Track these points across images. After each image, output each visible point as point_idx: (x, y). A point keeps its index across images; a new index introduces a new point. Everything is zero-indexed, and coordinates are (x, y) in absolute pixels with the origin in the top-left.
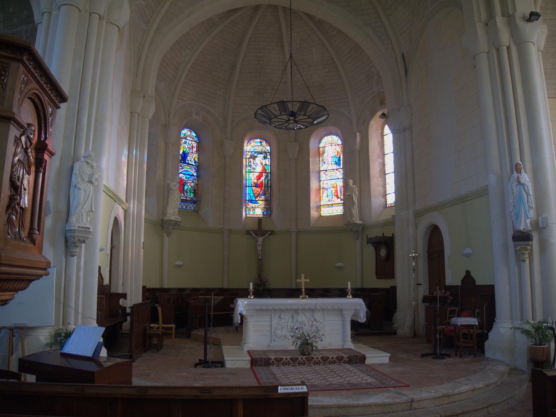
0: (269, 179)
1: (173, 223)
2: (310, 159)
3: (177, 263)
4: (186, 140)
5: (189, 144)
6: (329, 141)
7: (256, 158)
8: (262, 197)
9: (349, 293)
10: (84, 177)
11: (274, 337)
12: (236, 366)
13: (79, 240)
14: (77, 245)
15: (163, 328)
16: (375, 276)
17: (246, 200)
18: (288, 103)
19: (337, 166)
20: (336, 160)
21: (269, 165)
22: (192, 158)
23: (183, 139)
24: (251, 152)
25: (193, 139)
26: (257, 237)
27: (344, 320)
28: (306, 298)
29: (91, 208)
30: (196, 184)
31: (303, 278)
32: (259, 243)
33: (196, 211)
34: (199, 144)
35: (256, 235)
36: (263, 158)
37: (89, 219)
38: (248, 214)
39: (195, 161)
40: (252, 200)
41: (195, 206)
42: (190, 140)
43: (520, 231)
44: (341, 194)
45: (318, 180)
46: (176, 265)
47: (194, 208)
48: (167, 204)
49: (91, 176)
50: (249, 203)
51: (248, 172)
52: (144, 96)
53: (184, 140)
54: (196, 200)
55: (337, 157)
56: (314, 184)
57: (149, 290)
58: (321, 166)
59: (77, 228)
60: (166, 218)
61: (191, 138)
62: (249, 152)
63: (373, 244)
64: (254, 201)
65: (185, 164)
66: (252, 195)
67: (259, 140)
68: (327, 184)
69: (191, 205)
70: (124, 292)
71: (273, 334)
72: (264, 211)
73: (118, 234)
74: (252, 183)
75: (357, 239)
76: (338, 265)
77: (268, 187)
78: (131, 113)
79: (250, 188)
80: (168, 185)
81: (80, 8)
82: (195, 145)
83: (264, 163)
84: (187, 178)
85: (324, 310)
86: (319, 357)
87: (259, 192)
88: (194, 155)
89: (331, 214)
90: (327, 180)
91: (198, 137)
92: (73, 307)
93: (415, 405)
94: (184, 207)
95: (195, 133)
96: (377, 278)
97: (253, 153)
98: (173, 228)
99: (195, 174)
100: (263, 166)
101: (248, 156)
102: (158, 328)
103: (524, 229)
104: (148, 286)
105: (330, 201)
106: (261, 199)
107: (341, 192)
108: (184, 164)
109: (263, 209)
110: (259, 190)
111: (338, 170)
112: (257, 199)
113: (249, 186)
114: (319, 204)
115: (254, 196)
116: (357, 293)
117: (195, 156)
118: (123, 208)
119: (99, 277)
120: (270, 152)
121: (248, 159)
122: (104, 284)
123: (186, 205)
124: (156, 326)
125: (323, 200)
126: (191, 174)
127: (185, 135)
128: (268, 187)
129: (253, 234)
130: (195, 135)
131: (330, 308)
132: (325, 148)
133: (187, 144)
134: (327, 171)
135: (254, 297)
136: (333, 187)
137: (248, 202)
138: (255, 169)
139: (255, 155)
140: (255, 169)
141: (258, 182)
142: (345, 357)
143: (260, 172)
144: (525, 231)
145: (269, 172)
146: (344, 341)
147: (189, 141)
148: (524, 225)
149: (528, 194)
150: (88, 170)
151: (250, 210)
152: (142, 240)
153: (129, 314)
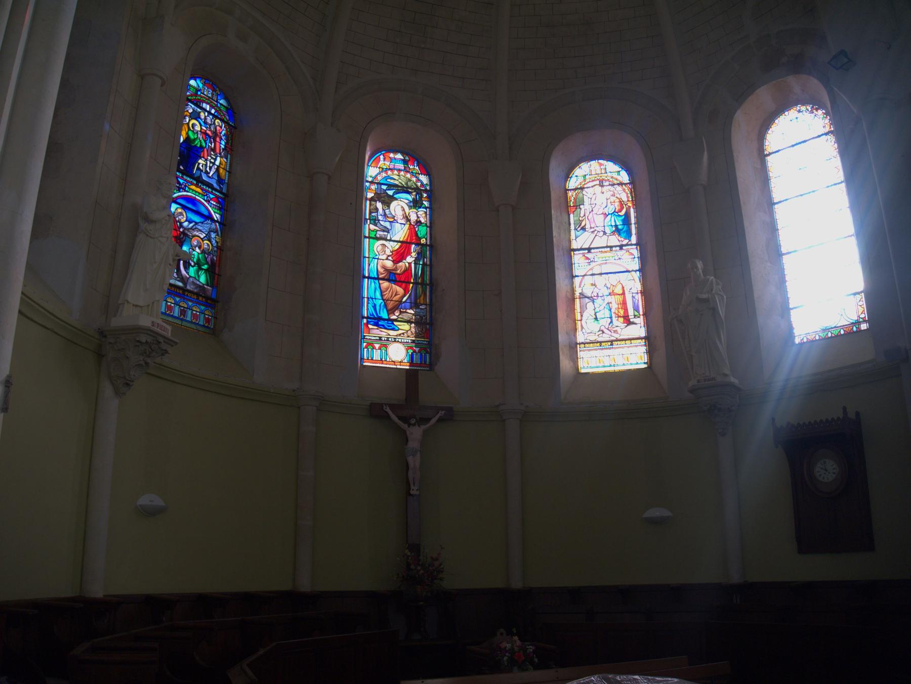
0: (428, 263)
2: (553, 212)
3: (145, 500)
6: (593, 173)
7: (393, 201)
8: (408, 311)
19: (620, 239)
20: (618, 223)
21: (428, 224)
24: (378, 184)
25: (220, 114)
26: (406, 426)
30: (217, 247)
32: (413, 444)
33: (213, 330)
35: (405, 420)
36: (412, 204)
38: (365, 358)
39: (219, 176)
40: (380, 319)
42: (209, 113)
44: (636, 313)
46: (140, 505)
47: (208, 320)
50: (370, 326)
51: (369, 237)
54: (214, 297)
55: (619, 214)
58: (573, 236)
60: (116, 322)
61: (212, 107)
62: (372, 183)
64: (385, 320)
65: (188, 179)
66: (379, 302)
67: (399, 156)
68: (592, 285)
72: (414, 351)
79: (373, 285)
83: (413, 218)
84: (190, 222)
87: (398, 297)
88: (218, 159)
89: (611, 369)
90: (593, 275)
94: (176, 312)
95: (226, 99)
97: (384, 187)
98: (142, 363)
99: (216, 216)
100: (410, 224)
105: (606, 331)
106: (405, 317)
107: (636, 309)
108: (187, 176)
109: (411, 348)
110: (400, 290)
111: (624, 248)
112: (394, 317)
113: (371, 278)
115: (386, 306)
117: (220, 163)
123: (181, 304)
125: (582, 327)
126: (206, 213)
127: (196, 95)
128: (423, 284)
129: (394, 417)
134: (592, 251)
137: (368, 323)
138: (388, 232)
139: (390, 193)
140: (388, 232)
143: (401, 240)
147: (206, 114)
151: (374, 348)
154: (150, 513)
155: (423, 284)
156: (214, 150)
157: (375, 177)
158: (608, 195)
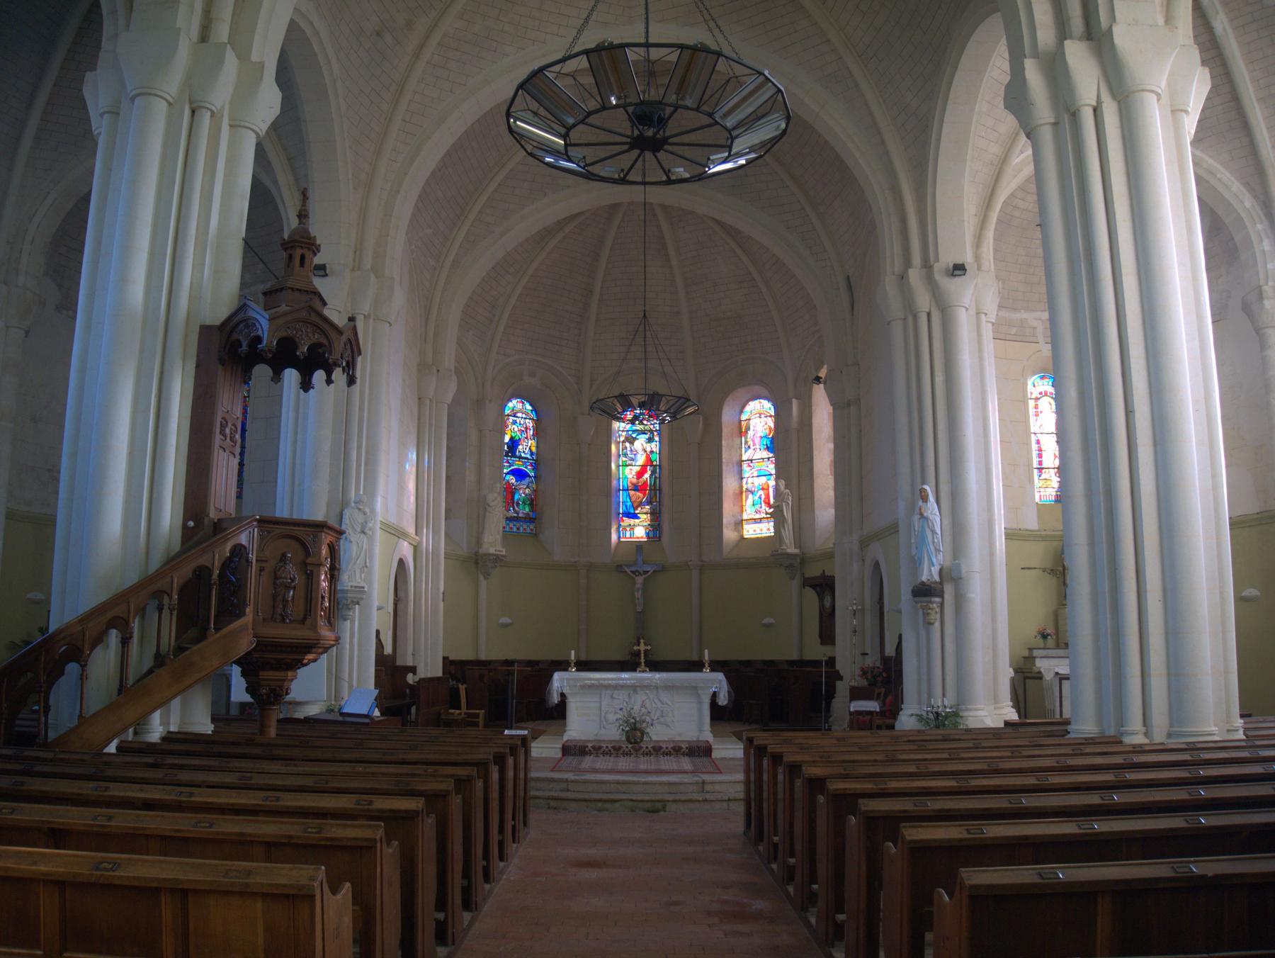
1: (492, 558)
2: (723, 442)
3: (503, 620)
4: (515, 419)
5: (520, 424)
9: (707, 665)
10: (356, 527)
11: (605, 723)
12: (543, 755)
13: (352, 601)
14: (350, 606)
15: (465, 714)
16: (819, 641)
17: (619, 514)
18: (631, 398)
22: (527, 446)
23: (510, 417)
26: (634, 576)
27: (700, 703)
28: (646, 671)
29: (365, 563)
31: (642, 644)
32: (638, 586)
33: (535, 535)
34: (538, 423)
37: (363, 576)
43: (923, 583)
45: (737, 477)
48: (483, 528)
49: (364, 525)
50: (624, 518)
52: (438, 371)
53: (511, 419)
54: (534, 517)
56: (729, 484)
57: (453, 663)
59: (349, 588)
60: (482, 551)
61: (523, 413)
62: (623, 431)
63: (813, 587)
66: (629, 504)
69: (525, 526)
70: (415, 665)
71: (603, 719)
73: (406, 582)
74: (629, 484)
75: (793, 579)
76: (766, 621)
77: (655, 490)
78: (420, 399)
80: (485, 498)
81: (338, 309)
82: (530, 424)
83: (648, 450)
85: (669, 687)
86: (650, 746)
88: (530, 441)
90: (753, 477)
91: (536, 412)
92: (347, 680)
93: (707, 788)
94: (515, 530)
96: (821, 644)
99: (532, 474)
101: (622, 439)
102: (460, 714)
103: (929, 580)
104: (452, 658)
106: (644, 510)
110: (641, 495)
112: (637, 512)
114: (740, 518)
116: (716, 666)
118: (410, 544)
119: (377, 643)
120: (659, 430)
121: (621, 444)
122: (385, 653)
124: (458, 711)
130: (530, 408)
131: (677, 684)
132: (751, 422)
133: (518, 425)
135: (577, 670)
136: (763, 489)
139: (634, 436)
141: (638, 483)
142: (684, 747)
144: (928, 583)
145: (656, 465)
146: (701, 730)
148: (930, 573)
149: (933, 532)
150: (360, 518)
151: (626, 530)
152: (442, 589)
156: (527, 438)
157: (625, 428)
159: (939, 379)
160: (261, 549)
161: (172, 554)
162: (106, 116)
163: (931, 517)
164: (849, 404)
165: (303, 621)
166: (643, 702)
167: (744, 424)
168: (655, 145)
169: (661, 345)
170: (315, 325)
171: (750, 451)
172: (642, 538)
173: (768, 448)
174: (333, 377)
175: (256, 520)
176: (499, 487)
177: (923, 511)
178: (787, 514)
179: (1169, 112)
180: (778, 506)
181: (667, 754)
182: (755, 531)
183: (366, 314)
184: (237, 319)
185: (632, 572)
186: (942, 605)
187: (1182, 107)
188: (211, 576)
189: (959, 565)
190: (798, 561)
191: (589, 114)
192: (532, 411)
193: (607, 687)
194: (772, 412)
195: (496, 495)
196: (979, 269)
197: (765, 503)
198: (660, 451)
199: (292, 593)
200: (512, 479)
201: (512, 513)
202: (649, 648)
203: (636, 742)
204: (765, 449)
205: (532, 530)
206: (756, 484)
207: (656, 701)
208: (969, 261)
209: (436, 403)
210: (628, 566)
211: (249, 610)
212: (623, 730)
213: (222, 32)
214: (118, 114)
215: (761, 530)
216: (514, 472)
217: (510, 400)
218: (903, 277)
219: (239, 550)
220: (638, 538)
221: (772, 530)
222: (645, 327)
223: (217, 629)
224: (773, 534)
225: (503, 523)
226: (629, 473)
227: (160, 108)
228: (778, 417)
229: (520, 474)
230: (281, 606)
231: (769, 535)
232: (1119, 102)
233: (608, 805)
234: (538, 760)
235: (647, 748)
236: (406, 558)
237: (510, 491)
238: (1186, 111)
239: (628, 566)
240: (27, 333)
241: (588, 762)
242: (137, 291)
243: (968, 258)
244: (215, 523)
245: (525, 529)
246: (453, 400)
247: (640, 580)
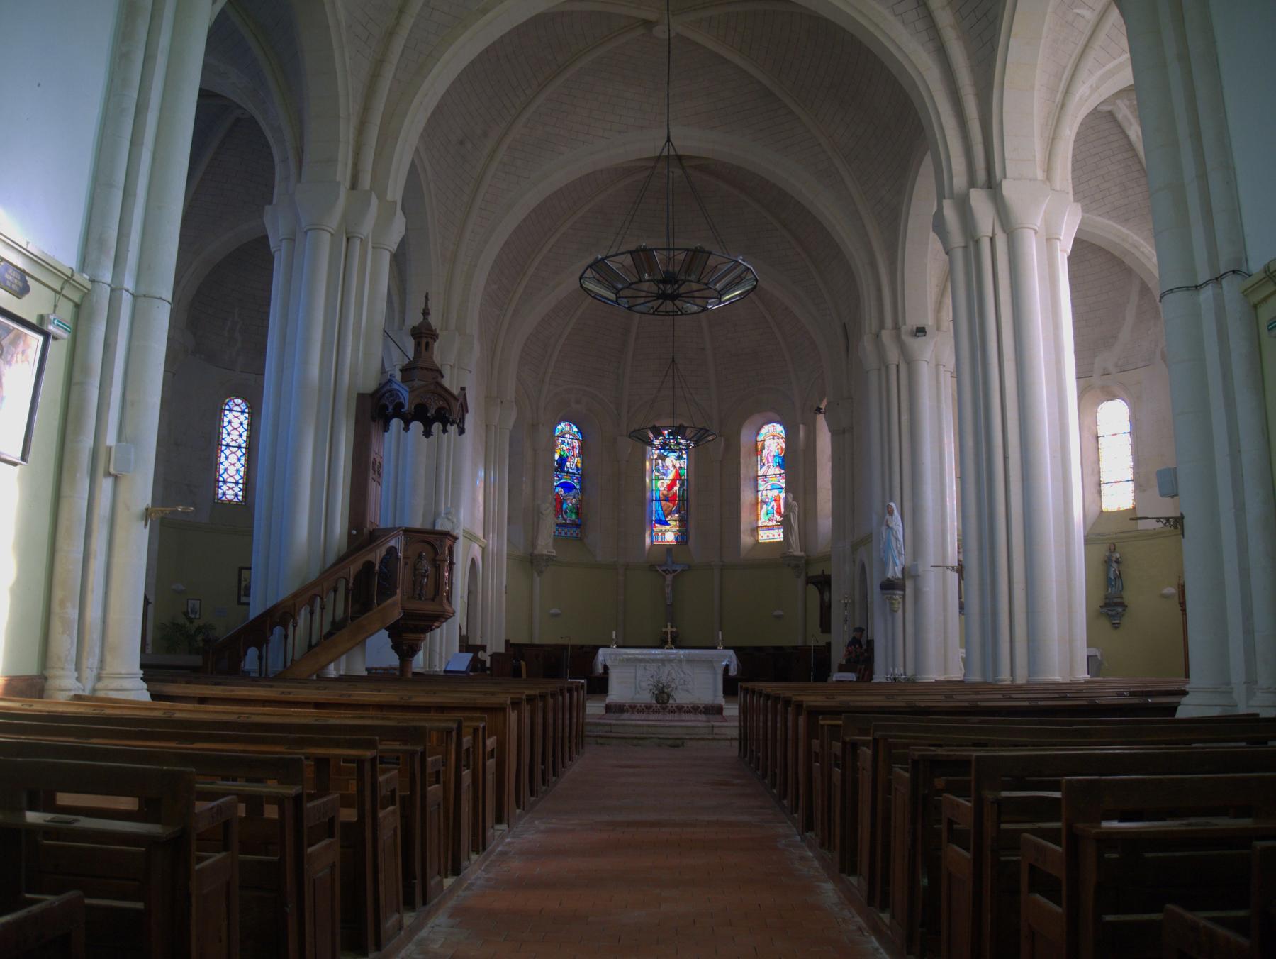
1: (545, 558)
2: (742, 461)
3: (553, 611)
11: (639, 689)
16: (820, 630)
22: (574, 463)
26: (664, 574)
31: (669, 627)
40: (661, 520)
41: (578, 531)
47: (578, 534)
51: (655, 480)
52: (502, 402)
56: (746, 496)
58: (759, 468)
60: (536, 552)
61: (570, 435)
63: (813, 583)
66: (661, 512)
69: (572, 531)
70: (484, 644)
74: (661, 496)
82: (576, 444)
83: (678, 466)
85: (690, 661)
91: (581, 434)
93: (716, 731)
94: (563, 534)
96: (822, 632)
99: (578, 487)
101: (655, 457)
106: (674, 518)
110: (671, 505)
112: (667, 519)
118: (480, 546)
127: (562, 432)
128: (683, 500)
136: (775, 500)
139: (665, 454)
144: (893, 579)
146: (715, 696)
148: (894, 571)
149: (897, 539)
152: (505, 584)
153: (488, 669)
154: (556, 615)
155: (683, 500)
156: (573, 456)
158: (776, 444)
159: (905, 418)
160: (405, 550)
161: (341, 554)
162: (284, 242)
163: (895, 527)
164: (844, 432)
165: (433, 600)
166: (669, 672)
167: (760, 444)
168: (674, 297)
169: (688, 388)
170: (440, 395)
171: (765, 468)
172: (672, 541)
173: (780, 466)
174: (447, 428)
175: (403, 530)
176: (551, 498)
177: (889, 522)
178: (794, 522)
179: (1045, 241)
180: (786, 515)
181: (687, 713)
182: (768, 536)
183: (452, 364)
184: (385, 389)
185: (664, 571)
186: (904, 596)
187: (1057, 237)
188: (375, 567)
189: (917, 565)
190: (803, 562)
191: (632, 284)
192: (578, 432)
193: (641, 660)
194: (783, 434)
195: (548, 505)
196: (938, 329)
197: (777, 512)
198: (687, 467)
199: (426, 580)
200: (561, 491)
201: (561, 520)
202: (674, 629)
203: (663, 703)
204: (777, 466)
205: (578, 534)
206: (770, 497)
207: (681, 673)
208: (930, 324)
209: (500, 429)
210: (659, 566)
211: (398, 591)
212: (653, 693)
213: (366, 182)
214: (294, 240)
215: (774, 536)
216: (563, 485)
217: (559, 423)
218: (878, 336)
219: (392, 551)
220: (668, 541)
221: (782, 536)
222: (674, 372)
223: (378, 604)
224: (782, 539)
225: (554, 528)
226: (661, 486)
227: (326, 237)
228: (788, 439)
229: (567, 487)
230: (419, 588)
231: (779, 540)
232: (1008, 234)
233: (641, 742)
234: (589, 715)
235: (672, 707)
236: (476, 557)
237: (559, 501)
238: (1059, 239)
239: (659, 566)
240: (174, 374)
241: (625, 716)
242: (315, 370)
243: (929, 322)
244: (370, 531)
245: (572, 534)
246: (514, 426)
247: (669, 577)
